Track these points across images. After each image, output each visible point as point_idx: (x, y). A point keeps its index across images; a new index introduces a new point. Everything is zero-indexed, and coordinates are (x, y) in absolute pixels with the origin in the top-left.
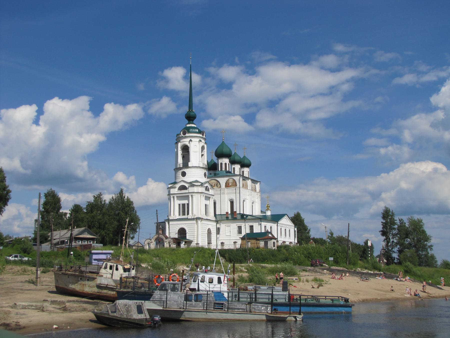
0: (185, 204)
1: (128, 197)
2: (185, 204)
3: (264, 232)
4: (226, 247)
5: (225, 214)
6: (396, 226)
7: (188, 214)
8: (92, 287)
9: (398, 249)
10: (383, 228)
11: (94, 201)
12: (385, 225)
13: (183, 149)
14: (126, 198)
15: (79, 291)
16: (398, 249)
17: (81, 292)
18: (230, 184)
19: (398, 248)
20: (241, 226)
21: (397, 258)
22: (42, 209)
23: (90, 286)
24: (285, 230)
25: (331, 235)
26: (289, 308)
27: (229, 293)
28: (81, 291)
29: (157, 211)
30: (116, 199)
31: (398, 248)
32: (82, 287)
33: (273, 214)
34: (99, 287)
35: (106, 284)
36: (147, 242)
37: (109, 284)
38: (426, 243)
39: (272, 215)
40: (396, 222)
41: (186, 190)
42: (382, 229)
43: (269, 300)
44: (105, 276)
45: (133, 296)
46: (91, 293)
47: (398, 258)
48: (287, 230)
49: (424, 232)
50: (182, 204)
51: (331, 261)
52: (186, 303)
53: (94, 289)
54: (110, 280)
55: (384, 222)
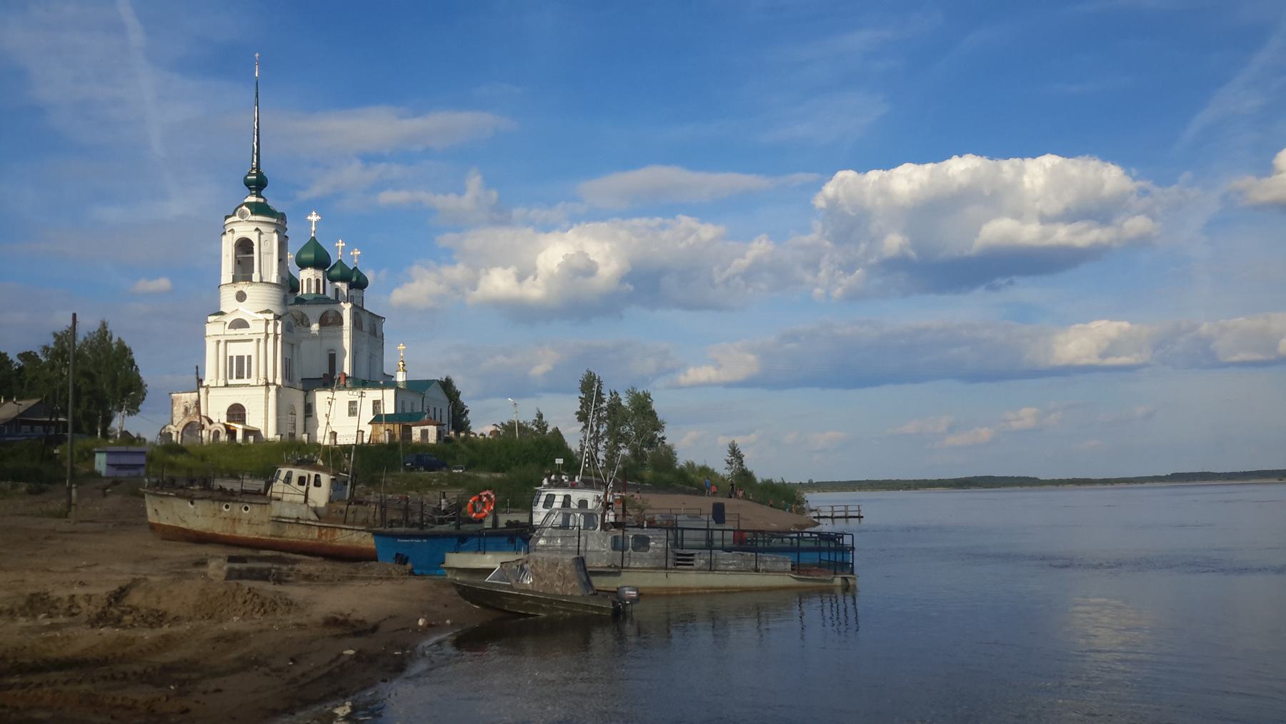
0: (243, 357)
1: (119, 339)
2: (243, 357)
3: (393, 412)
4: (341, 441)
5: (321, 378)
6: (605, 405)
7: (249, 376)
8: (258, 525)
9: (605, 445)
10: (581, 407)
11: (55, 343)
12: (585, 403)
13: (239, 246)
14: (115, 340)
15: (222, 534)
16: (605, 445)
17: (227, 536)
18: (330, 321)
19: (606, 443)
20: (374, 401)
21: (603, 460)
22: (45, 360)
23: (253, 522)
24: (435, 409)
25: (539, 418)
26: (796, 555)
27: (685, 531)
28: (227, 534)
29: (197, 368)
30: (92, 343)
31: (606, 443)
32: (231, 523)
33: (410, 379)
34: (278, 521)
35: (295, 516)
36: (219, 427)
37: (301, 517)
38: (655, 433)
39: (408, 382)
40: (604, 396)
41: (245, 327)
42: (580, 410)
43: (816, 544)
44: (286, 498)
45: (417, 541)
46: (256, 537)
47: (605, 459)
48: (437, 409)
49: (653, 414)
50: (237, 357)
51: (559, 464)
52: (756, 555)
53: (263, 528)
54: (304, 508)
55: (584, 396)
